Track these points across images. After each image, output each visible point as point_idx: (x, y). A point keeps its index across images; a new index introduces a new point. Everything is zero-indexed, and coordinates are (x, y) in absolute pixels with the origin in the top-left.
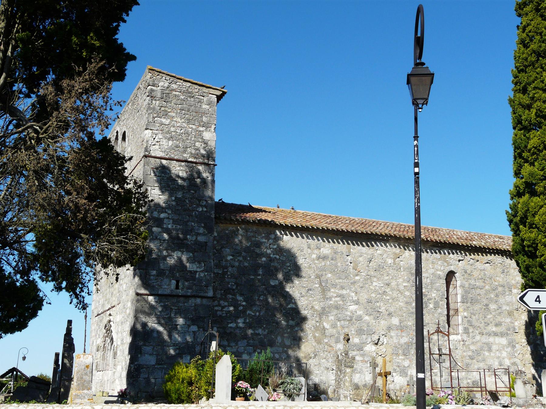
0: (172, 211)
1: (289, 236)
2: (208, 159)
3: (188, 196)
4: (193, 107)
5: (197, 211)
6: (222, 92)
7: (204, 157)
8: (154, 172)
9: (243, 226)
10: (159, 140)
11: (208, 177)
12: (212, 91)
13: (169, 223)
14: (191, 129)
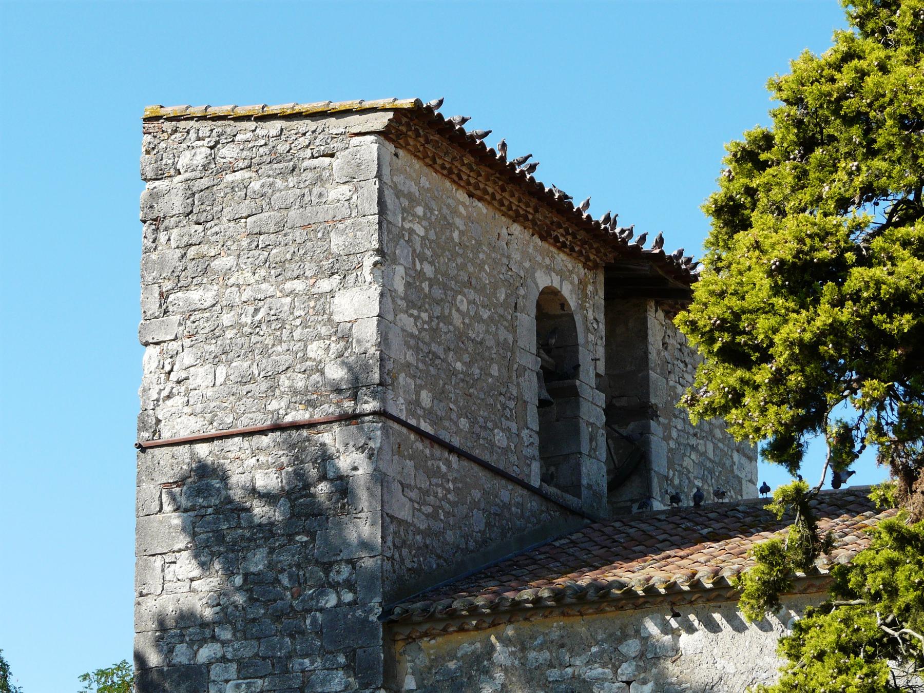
0: (235, 630)
1: (702, 632)
2: (355, 398)
3: (285, 558)
4: (293, 213)
5: (321, 610)
6: (390, 115)
7: (338, 391)
8: (173, 498)
9: (510, 631)
10: (183, 375)
11: (355, 469)
12: (356, 123)
13: (226, 677)
14: (289, 300)
